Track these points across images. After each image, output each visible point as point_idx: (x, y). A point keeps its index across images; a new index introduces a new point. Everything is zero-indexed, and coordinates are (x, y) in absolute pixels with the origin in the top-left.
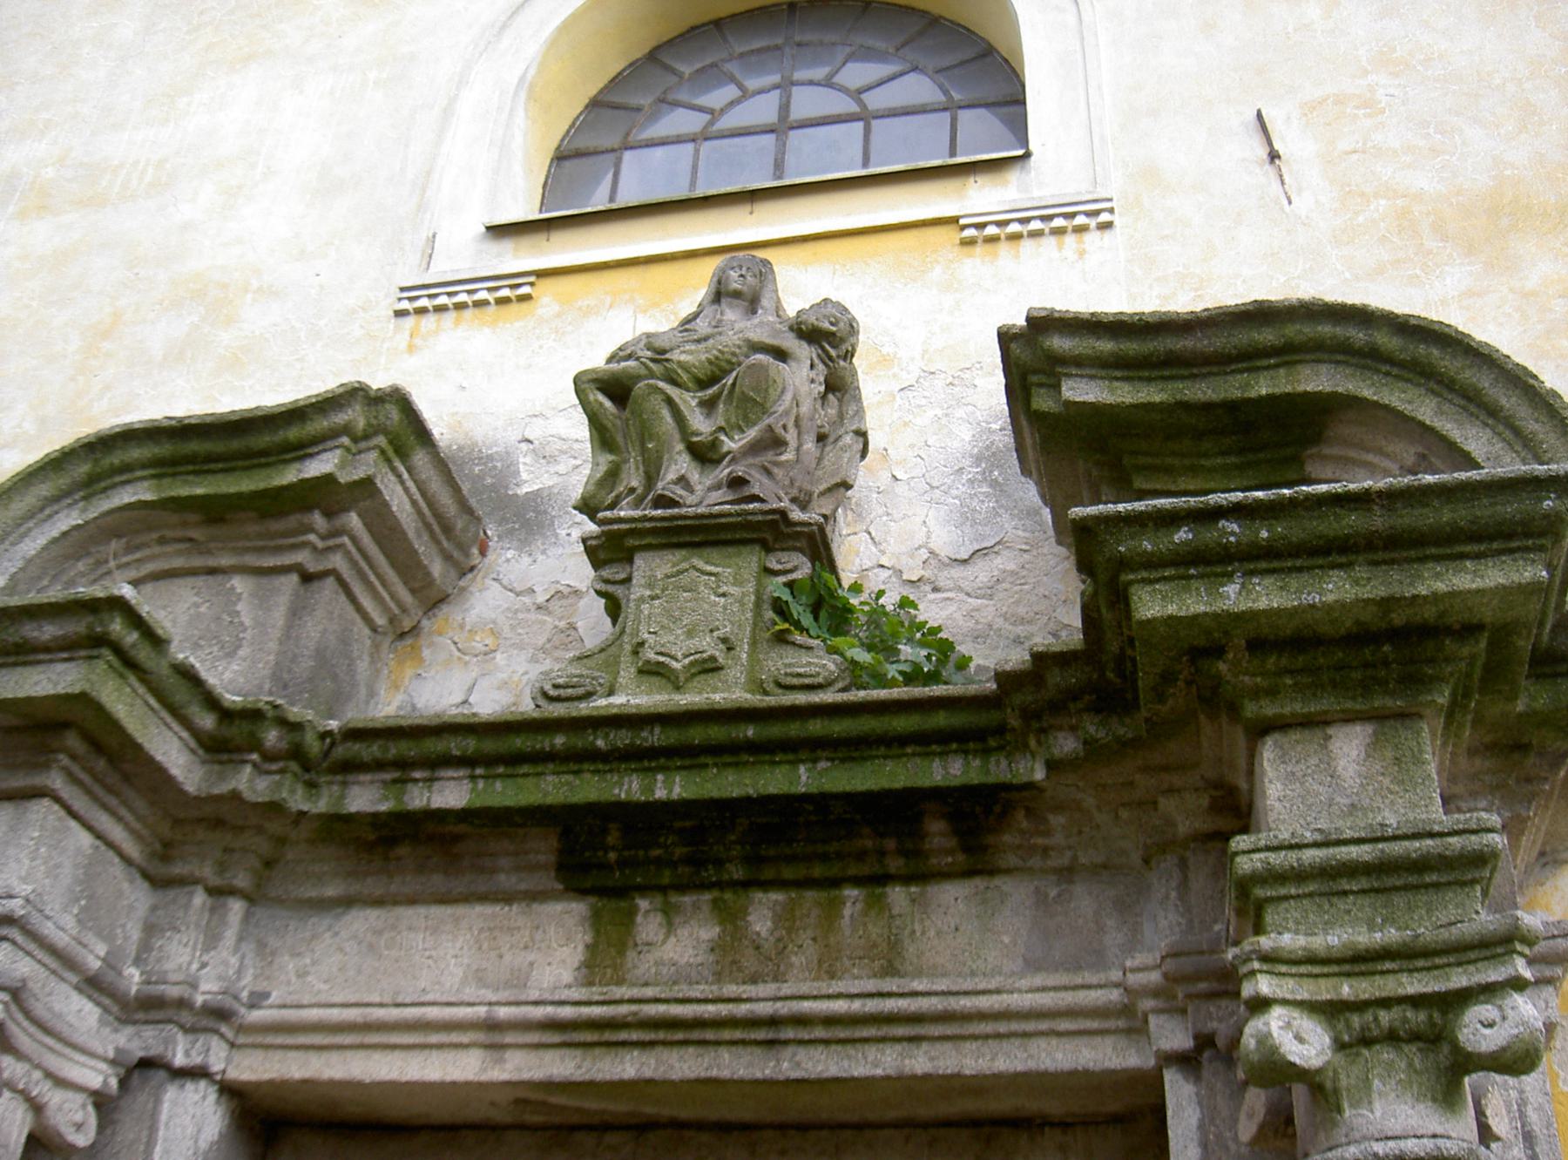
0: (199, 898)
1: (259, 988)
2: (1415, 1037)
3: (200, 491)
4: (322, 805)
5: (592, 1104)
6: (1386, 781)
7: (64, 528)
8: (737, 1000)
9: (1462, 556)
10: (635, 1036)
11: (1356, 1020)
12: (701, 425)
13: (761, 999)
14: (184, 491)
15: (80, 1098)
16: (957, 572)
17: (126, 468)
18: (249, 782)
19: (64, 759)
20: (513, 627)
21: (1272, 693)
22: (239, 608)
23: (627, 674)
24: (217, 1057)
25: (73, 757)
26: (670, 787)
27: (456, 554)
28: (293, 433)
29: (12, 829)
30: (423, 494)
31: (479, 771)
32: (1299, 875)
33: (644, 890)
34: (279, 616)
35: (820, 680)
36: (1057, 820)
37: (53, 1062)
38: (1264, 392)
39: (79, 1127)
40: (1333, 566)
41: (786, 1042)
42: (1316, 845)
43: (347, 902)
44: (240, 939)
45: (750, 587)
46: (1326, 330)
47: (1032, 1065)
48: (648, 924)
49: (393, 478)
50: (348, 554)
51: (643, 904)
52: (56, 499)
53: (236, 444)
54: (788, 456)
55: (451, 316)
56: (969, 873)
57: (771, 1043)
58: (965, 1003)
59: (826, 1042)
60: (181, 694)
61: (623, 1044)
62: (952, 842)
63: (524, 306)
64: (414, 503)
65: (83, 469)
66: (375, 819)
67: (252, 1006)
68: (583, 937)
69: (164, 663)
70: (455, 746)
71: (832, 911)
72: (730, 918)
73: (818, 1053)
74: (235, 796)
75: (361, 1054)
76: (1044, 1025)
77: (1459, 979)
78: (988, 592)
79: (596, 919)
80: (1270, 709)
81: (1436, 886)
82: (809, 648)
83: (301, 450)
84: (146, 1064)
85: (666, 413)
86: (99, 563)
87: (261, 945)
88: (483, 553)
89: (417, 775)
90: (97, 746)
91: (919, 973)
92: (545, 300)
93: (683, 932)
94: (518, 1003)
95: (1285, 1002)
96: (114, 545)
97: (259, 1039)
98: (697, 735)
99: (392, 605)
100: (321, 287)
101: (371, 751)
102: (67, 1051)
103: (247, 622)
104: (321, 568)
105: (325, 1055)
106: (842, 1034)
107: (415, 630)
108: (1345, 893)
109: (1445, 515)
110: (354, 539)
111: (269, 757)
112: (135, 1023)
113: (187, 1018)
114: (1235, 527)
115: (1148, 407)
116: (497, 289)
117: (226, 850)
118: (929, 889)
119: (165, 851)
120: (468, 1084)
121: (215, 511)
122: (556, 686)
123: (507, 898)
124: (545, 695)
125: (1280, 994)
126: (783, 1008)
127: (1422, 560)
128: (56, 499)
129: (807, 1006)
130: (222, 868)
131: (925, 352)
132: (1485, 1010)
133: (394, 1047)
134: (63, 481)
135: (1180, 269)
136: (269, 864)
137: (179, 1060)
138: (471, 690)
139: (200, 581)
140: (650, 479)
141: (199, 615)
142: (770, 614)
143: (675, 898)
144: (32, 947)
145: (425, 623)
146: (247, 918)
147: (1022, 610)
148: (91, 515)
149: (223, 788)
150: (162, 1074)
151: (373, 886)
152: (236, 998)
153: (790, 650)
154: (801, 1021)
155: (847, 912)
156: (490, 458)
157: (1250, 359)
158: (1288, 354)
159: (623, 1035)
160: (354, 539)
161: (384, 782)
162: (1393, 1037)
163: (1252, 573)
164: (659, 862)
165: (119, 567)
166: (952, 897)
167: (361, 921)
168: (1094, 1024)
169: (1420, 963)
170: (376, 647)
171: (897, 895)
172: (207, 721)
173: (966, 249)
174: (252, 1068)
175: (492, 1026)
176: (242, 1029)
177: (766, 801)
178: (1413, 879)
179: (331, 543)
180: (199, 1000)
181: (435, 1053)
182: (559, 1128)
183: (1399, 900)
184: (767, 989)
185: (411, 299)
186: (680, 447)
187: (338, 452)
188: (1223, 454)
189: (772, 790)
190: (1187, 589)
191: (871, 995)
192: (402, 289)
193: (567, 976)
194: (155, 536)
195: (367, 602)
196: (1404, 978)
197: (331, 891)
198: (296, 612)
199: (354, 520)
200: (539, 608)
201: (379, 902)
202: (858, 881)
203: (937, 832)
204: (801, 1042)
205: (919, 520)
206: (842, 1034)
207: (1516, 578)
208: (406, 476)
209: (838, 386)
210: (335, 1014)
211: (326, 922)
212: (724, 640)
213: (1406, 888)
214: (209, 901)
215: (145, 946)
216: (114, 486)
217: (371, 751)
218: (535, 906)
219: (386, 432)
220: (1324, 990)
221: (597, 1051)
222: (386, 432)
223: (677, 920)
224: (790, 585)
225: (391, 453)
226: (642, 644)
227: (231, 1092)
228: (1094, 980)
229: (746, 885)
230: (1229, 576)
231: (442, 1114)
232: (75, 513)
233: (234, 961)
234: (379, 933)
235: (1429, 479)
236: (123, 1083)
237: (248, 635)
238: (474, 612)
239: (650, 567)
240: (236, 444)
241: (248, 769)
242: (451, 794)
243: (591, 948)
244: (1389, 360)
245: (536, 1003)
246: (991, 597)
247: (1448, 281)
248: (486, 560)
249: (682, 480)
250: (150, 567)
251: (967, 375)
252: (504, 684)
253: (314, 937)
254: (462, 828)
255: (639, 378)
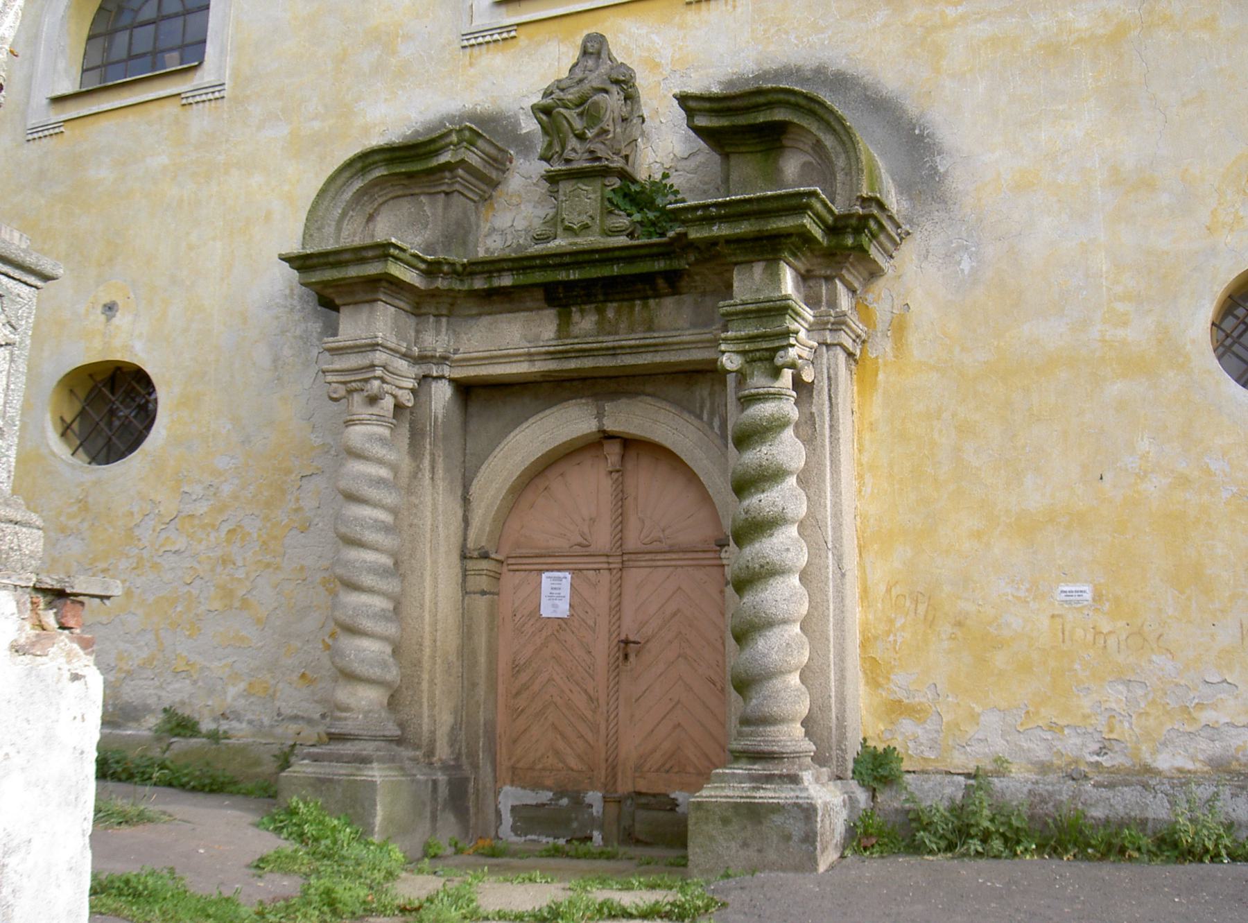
0: (432, 319)
1: (455, 348)
2: (766, 359)
3: (403, 170)
4: (466, 287)
5: (566, 375)
6: (767, 281)
7: (357, 188)
8: (602, 342)
9: (781, 216)
10: (573, 355)
11: (750, 355)
12: (578, 125)
13: (609, 341)
14: (397, 170)
15: (407, 391)
16: (684, 163)
17: (374, 163)
18: (440, 283)
19: (382, 289)
20: (526, 193)
21: (735, 255)
22: (425, 208)
23: (560, 231)
24: (447, 371)
25: (385, 288)
26: (574, 275)
27: (500, 167)
28: (432, 147)
29: (370, 313)
30: (484, 153)
31: (514, 272)
32: (736, 314)
33: (573, 305)
34: (440, 211)
35: (624, 228)
36: (697, 278)
37: (397, 383)
38: (761, 120)
39: (409, 400)
40: (745, 220)
41: (619, 354)
42: (740, 305)
43: (480, 315)
44: (447, 330)
45: (599, 194)
46: (781, 96)
47: (690, 358)
48: (576, 317)
49: (470, 153)
50: (460, 183)
51: (574, 309)
52: (352, 177)
53: (412, 153)
54: (610, 136)
55: (484, 47)
56: (673, 294)
57: (614, 355)
58: (670, 340)
59: (630, 353)
60: (415, 262)
61: (571, 357)
62: (666, 285)
63: (514, 41)
64: (480, 157)
65: (359, 165)
66: (484, 290)
67: (454, 354)
68: (556, 322)
69: (407, 255)
70: (505, 265)
71: (632, 308)
72: (600, 312)
73: (628, 357)
74: (437, 288)
75: (491, 366)
76: (694, 346)
77: (777, 344)
78: (695, 171)
79: (560, 315)
80: (734, 260)
81: (774, 315)
82: (620, 215)
83: (437, 153)
84: (425, 377)
85: (565, 123)
86: (371, 196)
87: (454, 331)
88: (511, 162)
89: (495, 275)
90: (391, 283)
91: (659, 330)
92: (522, 37)
93: (587, 318)
94: (537, 347)
95: (729, 352)
96: (376, 189)
97: (458, 364)
98: (580, 258)
99: (480, 192)
100: (429, 33)
101: (479, 268)
102: (404, 379)
103: (429, 214)
104: (451, 190)
105: (480, 367)
106: (635, 351)
107: (491, 197)
108: (750, 318)
109: (775, 205)
110: (461, 178)
111: (446, 274)
112: (419, 364)
113: (434, 361)
114: (714, 210)
115: (723, 127)
116: (502, 33)
117: (437, 303)
118: (662, 300)
119: (418, 305)
120: (525, 373)
121: (410, 176)
122: (538, 235)
123: (530, 310)
124: (534, 238)
125: (728, 349)
126: (616, 344)
127: (771, 217)
128: (352, 177)
129: (623, 343)
130: (437, 308)
131: (672, 60)
132: (782, 353)
133: (501, 363)
134: (353, 170)
135: (773, 15)
136: (452, 305)
137: (435, 374)
138: (513, 221)
139: (409, 199)
140: (563, 148)
141: (411, 212)
142: (607, 203)
143: (583, 307)
144: (385, 350)
145: (494, 193)
146: (448, 322)
147: (706, 179)
148: (366, 182)
149: (432, 287)
150: (430, 379)
151: (487, 309)
152: (449, 352)
153: (614, 217)
154: (622, 347)
155: (637, 309)
156: (509, 117)
157: (757, 108)
158: (770, 105)
159: (570, 355)
160: (461, 178)
161: (485, 278)
162: (760, 360)
163: (721, 223)
164: (577, 296)
165: (379, 196)
166: (669, 302)
167: (485, 320)
168: (708, 345)
169: (767, 339)
170: (477, 208)
171: (652, 302)
172: (423, 266)
173: (689, 7)
174: (459, 373)
175: (530, 354)
176: (453, 361)
177: (604, 278)
178: (767, 314)
179: (453, 180)
180: (438, 355)
181: (514, 364)
182: (558, 381)
183: (764, 320)
184: (611, 338)
185: (468, 40)
186: (571, 135)
187: (450, 152)
188: (754, 138)
189: (606, 274)
190: (703, 228)
191: (640, 339)
192: (463, 35)
193: (552, 335)
194: (390, 184)
195: (470, 195)
196: (763, 343)
197: (474, 312)
198: (446, 207)
199: (460, 172)
200: (534, 184)
201: (490, 314)
202: (640, 299)
203: (661, 282)
204: (623, 354)
205: (670, 141)
206: (635, 351)
207: (796, 223)
208: (476, 150)
209: (630, 97)
210: (481, 354)
211: (474, 322)
212: (591, 216)
213: (766, 316)
214: (435, 319)
215: (417, 338)
216: (372, 170)
217: (479, 268)
218: (540, 312)
219: (465, 141)
220: (740, 347)
221: (563, 360)
222: (465, 141)
223: (585, 314)
224: (613, 190)
225: (468, 146)
226: (564, 219)
227: (451, 380)
228: (707, 331)
229: (605, 301)
230: (715, 224)
231: (522, 380)
232: (360, 181)
233: (446, 338)
234: (491, 324)
235: (769, 193)
236: (418, 384)
237: (430, 219)
238: (511, 187)
239: (565, 187)
240: (412, 153)
241: (440, 279)
242: (506, 281)
243: (559, 325)
244: (802, 107)
245: (542, 346)
246: (696, 173)
247: (877, 19)
248: (513, 165)
249: (574, 150)
250: (391, 195)
251: (688, 72)
252: (525, 218)
253: (471, 327)
254: (512, 290)
255: (554, 108)
